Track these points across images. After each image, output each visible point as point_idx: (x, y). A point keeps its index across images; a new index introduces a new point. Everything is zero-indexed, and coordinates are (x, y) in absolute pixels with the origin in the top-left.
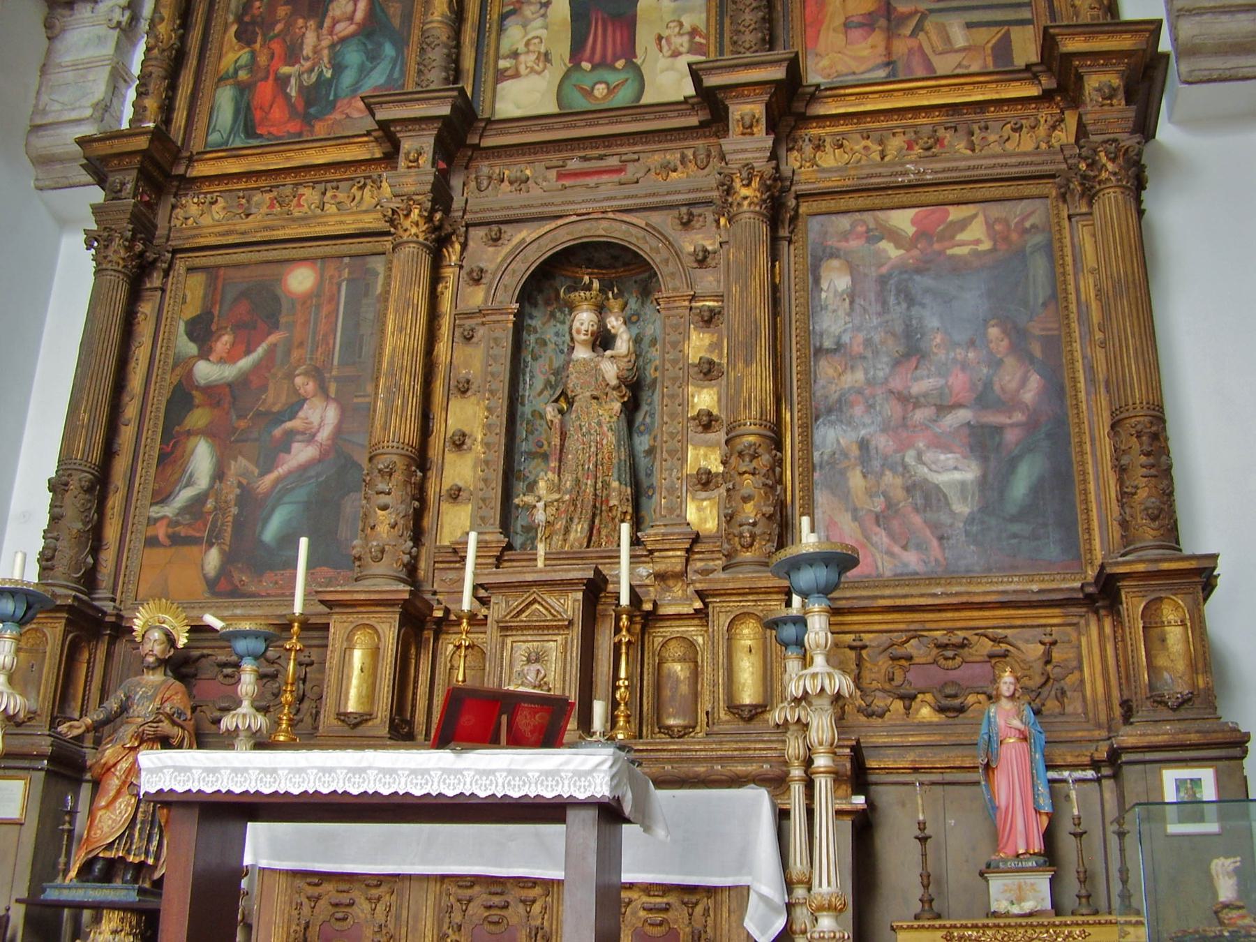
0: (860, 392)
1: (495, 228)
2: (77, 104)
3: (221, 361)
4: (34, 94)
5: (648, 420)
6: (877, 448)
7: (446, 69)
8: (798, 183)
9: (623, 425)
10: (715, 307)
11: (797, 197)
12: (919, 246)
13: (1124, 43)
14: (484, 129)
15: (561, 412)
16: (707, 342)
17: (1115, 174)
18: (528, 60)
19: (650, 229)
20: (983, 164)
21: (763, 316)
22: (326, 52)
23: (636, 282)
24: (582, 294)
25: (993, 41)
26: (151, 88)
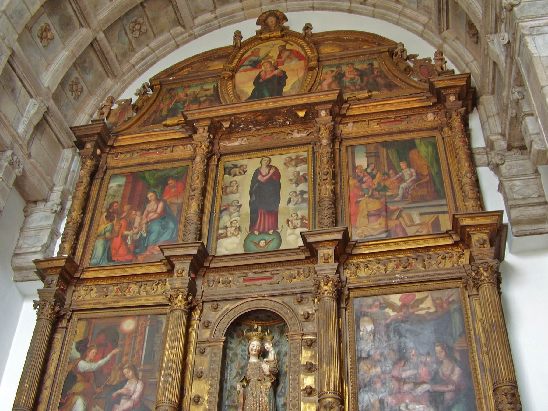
0: (379, 377)
1: (215, 303)
2: (35, 245)
3: (91, 361)
4: (16, 240)
5: (283, 390)
6: (387, 403)
7: (196, 234)
8: (349, 283)
9: (272, 392)
10: (313, 339)
11: (349, 289)
12: (403, 310)
13: (488, 220)
14: (212, 260)
15: (244, 387)
16: (309, 355)
17: (487, 277)
18: (231, 230)
19: (284, 304)
20: (430, 274)
21: (334, 343)
22: (144, 225)
23: (278, 327)
24: (254, 333)
25: (432, 221)
26: (68, 239)
